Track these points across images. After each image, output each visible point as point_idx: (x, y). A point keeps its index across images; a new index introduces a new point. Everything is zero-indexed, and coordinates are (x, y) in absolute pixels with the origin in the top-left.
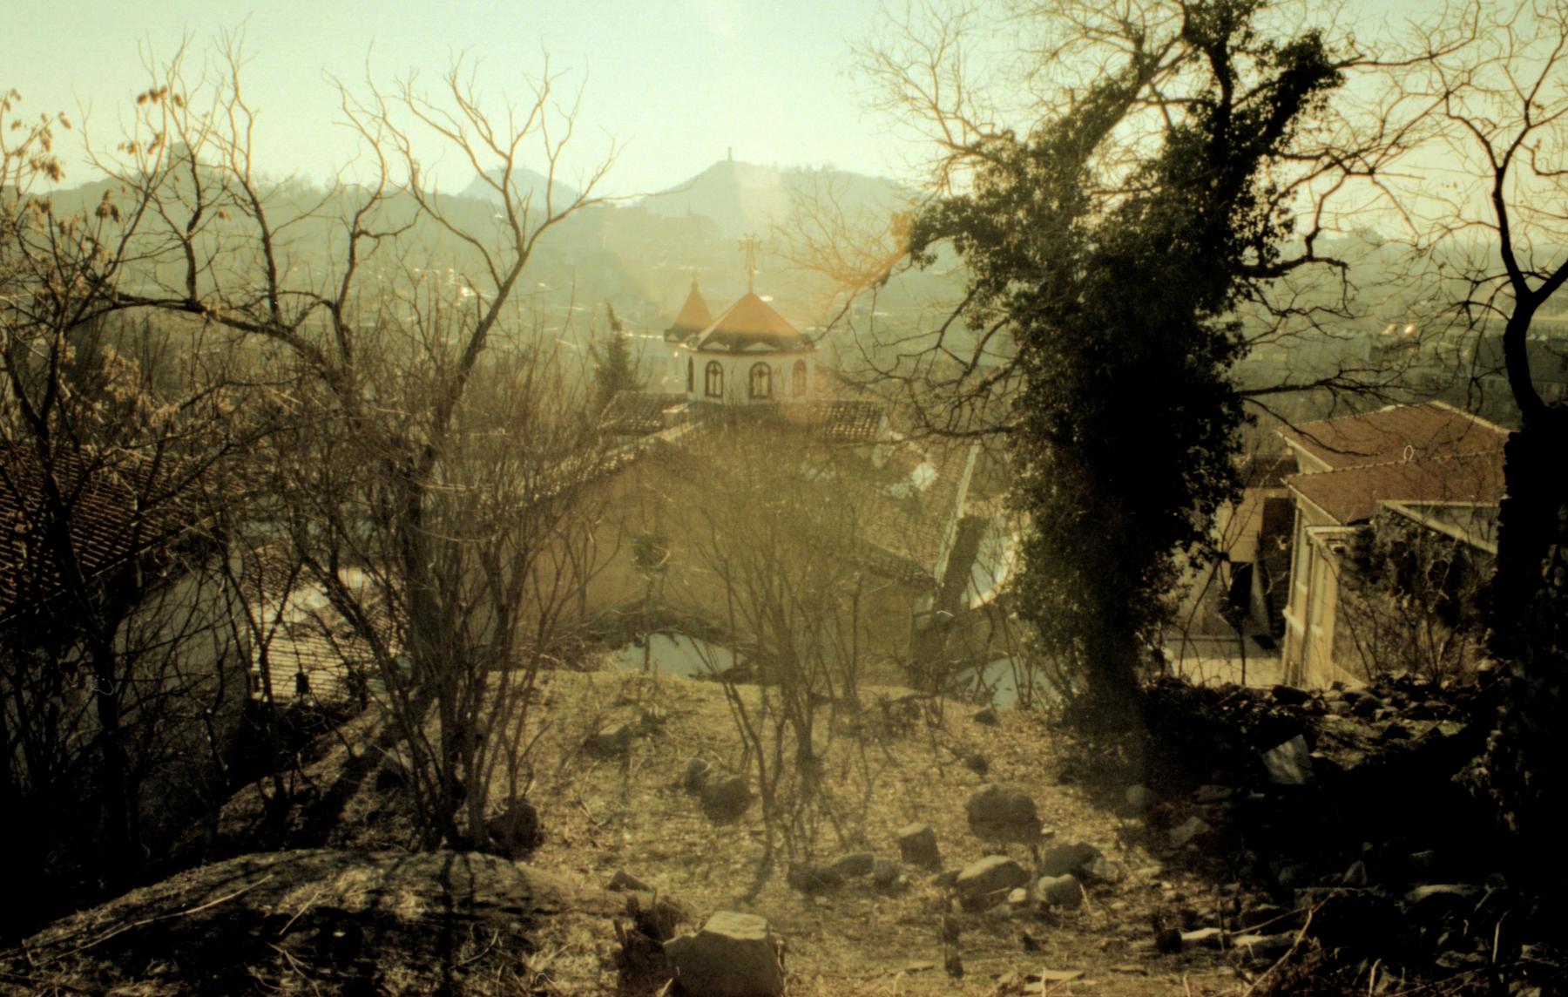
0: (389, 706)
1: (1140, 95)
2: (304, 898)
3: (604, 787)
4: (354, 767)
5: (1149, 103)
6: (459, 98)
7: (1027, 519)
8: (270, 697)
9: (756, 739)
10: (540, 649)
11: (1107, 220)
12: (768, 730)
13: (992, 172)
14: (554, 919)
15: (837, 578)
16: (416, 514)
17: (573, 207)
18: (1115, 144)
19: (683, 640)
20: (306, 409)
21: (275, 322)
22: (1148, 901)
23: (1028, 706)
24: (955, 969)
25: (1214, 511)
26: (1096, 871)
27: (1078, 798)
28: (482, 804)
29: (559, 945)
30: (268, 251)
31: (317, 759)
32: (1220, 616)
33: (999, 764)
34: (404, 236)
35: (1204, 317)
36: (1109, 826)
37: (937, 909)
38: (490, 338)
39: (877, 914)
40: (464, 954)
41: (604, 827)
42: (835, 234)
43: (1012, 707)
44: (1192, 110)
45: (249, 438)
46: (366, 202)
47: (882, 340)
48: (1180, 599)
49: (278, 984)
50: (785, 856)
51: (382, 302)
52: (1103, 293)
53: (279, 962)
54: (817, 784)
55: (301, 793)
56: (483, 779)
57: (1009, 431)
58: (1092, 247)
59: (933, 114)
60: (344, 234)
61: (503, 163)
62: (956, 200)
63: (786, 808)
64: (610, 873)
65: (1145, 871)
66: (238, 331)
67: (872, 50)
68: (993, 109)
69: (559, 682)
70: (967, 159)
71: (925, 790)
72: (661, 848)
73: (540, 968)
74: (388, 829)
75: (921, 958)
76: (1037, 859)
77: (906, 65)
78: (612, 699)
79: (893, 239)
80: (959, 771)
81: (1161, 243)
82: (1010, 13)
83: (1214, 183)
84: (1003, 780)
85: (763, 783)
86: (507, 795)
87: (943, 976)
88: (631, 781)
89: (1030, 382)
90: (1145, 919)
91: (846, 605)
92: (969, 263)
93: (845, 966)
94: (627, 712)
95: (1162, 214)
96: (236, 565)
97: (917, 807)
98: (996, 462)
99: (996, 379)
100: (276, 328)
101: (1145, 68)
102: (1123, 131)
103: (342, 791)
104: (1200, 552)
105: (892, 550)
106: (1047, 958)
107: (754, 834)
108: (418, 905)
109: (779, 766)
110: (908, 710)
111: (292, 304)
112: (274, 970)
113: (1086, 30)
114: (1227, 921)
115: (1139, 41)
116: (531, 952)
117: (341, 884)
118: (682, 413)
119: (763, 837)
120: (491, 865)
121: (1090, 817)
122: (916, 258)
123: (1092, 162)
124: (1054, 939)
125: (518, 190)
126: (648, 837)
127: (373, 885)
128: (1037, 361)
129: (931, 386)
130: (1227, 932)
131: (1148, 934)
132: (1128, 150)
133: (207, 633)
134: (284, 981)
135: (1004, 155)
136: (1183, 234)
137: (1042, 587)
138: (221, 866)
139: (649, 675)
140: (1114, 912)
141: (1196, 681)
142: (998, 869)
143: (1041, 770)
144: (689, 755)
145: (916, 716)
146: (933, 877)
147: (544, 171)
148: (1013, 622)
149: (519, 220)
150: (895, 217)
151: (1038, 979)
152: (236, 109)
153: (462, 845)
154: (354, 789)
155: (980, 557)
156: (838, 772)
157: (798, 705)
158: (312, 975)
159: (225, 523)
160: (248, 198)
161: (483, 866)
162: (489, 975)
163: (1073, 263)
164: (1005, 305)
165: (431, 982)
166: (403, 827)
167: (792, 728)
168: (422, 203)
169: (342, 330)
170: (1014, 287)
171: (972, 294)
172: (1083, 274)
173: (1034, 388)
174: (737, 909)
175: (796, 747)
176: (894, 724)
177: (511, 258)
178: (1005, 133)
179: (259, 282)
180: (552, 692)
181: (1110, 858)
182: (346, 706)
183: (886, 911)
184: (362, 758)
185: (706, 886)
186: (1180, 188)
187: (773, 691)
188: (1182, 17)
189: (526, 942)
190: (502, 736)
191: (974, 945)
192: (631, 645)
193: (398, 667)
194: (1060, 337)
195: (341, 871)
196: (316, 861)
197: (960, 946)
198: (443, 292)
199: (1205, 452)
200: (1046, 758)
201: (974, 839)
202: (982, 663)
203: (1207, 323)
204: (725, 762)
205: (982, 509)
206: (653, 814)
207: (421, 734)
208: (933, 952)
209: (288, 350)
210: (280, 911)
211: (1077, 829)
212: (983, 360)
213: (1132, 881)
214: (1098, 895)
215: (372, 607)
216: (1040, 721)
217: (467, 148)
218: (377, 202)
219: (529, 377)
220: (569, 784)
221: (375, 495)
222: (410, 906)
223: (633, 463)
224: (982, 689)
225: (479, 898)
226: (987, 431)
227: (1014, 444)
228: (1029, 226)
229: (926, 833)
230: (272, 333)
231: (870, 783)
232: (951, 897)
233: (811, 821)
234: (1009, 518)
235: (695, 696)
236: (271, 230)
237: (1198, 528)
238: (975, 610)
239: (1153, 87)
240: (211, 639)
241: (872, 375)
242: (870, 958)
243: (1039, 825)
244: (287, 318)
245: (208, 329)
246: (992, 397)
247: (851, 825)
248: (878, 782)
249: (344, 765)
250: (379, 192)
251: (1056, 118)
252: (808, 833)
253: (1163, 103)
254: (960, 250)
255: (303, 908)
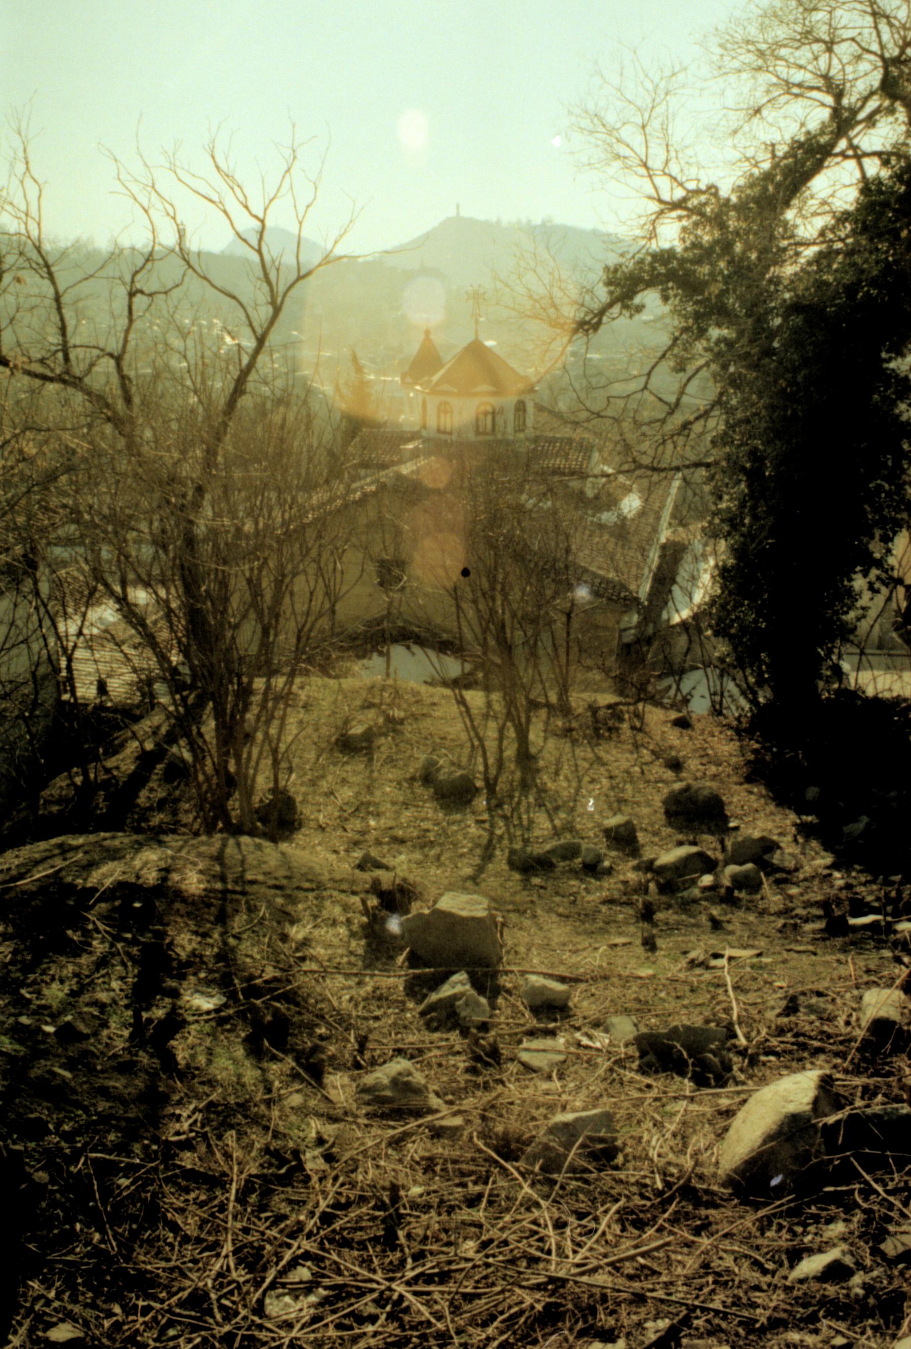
0: (171, 708)
1: (837, 150)
2: (108, 874)
3: (353, 779)
4: (146, 760)
5: (846, 157)
6: (218, 167)
7: (722, 545)
8: (76, 698)
9: (480, 739)
10: (297, 660)
11: (802, 270)
12: (491, 732)
13: (696, 224)
14: (311, 895)
15: (554, 598)
16: (190, 541)
17: (320, 265)
18: (812, 197)
19: (416, 649)
20: (96, 452)
21: (67, 373)
22: (821, 889)
23: (719, 713)
24: (650, 944)
25: (892, 540)
26: (775, 861)
27: (762, 796)
28: (249, 792)
29: (316, 917)
30: (59, 309)
31: (116, 752)
32: (894, 635)
33: (693, 764)
34: (175, 293)
35: (889, 360)
36: (788, 822)
37: (635, 891)
38: (250, 386)
39: (584, 894)
40: (238, 922)
41: (353, 814)
42: (552, 286)
43: (705, 713)
44: (886, 163)
45: (51, 477)
46: (140, 263)
47: (594, 381)
48: (859, 619)
49: (90, 945)
50: (506, 842)
51: (157, 352)
52: (796, 340)
53: (91, 927)
54: (534, 779)
55: (103, 781)
56: (251, 771)
57: (708, 466)
58: (787, 296)
59: (642, 171)
60: (122, 292)
61: (257, 224)
62: (663, 251)
63: (507, 800)
64: (358, 854)
65: (819, 862)
66: (38, 382)
67: (586, 112)
68: (700, 166)
69: (314, 688)
70: (675, 214)
71: (628, 786)
72: (400, 833)
73: (300, 936)
74: (175, 813)
75: (620, 934)
76: (724, 849)
77: (618, 126)
78: (358, 702)
79: (605, 289)
80: (658, 770)
81: (851, 290)
82: (716, 73)
83: (904, 234)
84: (696, 779)
85: (486, 780)
86: (271, 785)
87: (640, 950)
88: (375, 774)
89: (727, 422)
90: (817, 904)
91: (559, 626)
92: (674, 311)
93: (556, 940)
94: (371, 713)
95: (854, 265)
96: (44, 588)
97: (621, 801)
98: (695, 494)
99: (697, 419)
100: (69, 379)
101: (843, 121)
102: (820, 185)
103: (138, 779)
104: (878, 578)
105: (602, 573)
106: (730, 937)
107: (479, 822)
108: (199, 882)
109: (500, 762)
110: (613, 715)
111: (81, 356)
112: (87, 934)
113: (788, 86)
114: (889, 909)
115: (839, 96)
116: (293, 922)
117: (137, 863)
118: (416, 448)
119: (487, 825)
120: (259, 847)
121: (772, 814)
122: (626, 307)
123: (790, 215)
124: (737, 919)
125: (272, 249)
126: (391, 823)
127: (163, 864)
128: (734, 402)
129: (637, 424)
130: (889, 919)
131: (819, 917)
132: (824, 203)
133: (23, 646)
134: (95, 943)
135: (708, 209)
136: (873, 283)
137: (735, 607)
138: (43, 845)
139: (390, 682)
140: (791, 898)
141: (870, 692)
142: (689, 858)
143: (729, 770)
144: (424, 752)
145: (621, 719)
146: (634, 862)
147: (294, 230)
148: (708, 638)
149: (273, 276)
150: (607, 269)
151: (722, 956)
152: (28, 181)
153: (236, 830)
154: (147, 780)
155: (679, 579)
156: (552, 769)
157: (517, 710)
158: (117, 938)
159: (33, 549)
160: (41, 261)
161: (252, 848)
162: (259, 942)
163: (770, 311)
164: (706, 350)
165: (212, 946)
166: (187, 811)
167: (512, 730)
168: (188, 263)
169: (124, 379)
170: (715, 333)
171: (676, 339)
172: (778, 321)
173: (731, 427)
174: (465, 889)
175: (515, 746)
176: (602, 727)
177: (265, 312)
178: (710, 187)
179: (54, 339)
180: (308, 697)
181: (789, 851)
182: (138, 706)
183: (595, 893)
184: (152, 752)
185: (438, 867)
186: (871, 240)
187: (496, 696)
188: (881, 71)
189: (288, 914)
190: (266, 734)
191: (667, 924)
192: (375, 655)
193: (179, 674)
194: (757, 378)
195: (138, 851)
196: (117, 843)
197: (655, 925)
198: (208, 343)
199: (887, 486)
200: (734, 760)
201: (669, 830)
202: (680, 672)
203: (892, 365)
204: (455, 760)
205: (682, 534)
206: (394, 803)
207: (200, 735)
208: (632, 929)
209: (79, 397)
210: (89, 885)
211: (759, 823)
212: (685, 399)
213: (807, 871)
214: (778, 882)
215: (155, 623)
216: (730, 727)
217: (225, 212)
218: (149, 265)
219: (284, 419)
220: (323, 777)
221: (156, 524)
222: (193, 882)
223: (374, 494)
224: (679, 697)
225: (249, 876)
226: (688, 467)
227: (712, 478)
228: (729, 276)
229: (628, 824)
230: (64, 382)
231: (580, 781)
232: (648, 881)
233: (528, 812)
234: (706, 545)
235: (429, 701)
236: (61, 290)
237: (877, 555)
238: (673, 627)
239: (850, 140)
240: (26, 652)
241: (584, 415)
242: (578, 934)
243: (726, 819)
244: (77, 370)
245: (13, 381)
246: (692, 436)
247: (563, 815)
248: (587, 779)
249: (137, 758)
250: (151, 254)
251: (756, 172)
252: (525, 822)
253: (859, 156)
254: (666, 298)
255: (108, 882)
